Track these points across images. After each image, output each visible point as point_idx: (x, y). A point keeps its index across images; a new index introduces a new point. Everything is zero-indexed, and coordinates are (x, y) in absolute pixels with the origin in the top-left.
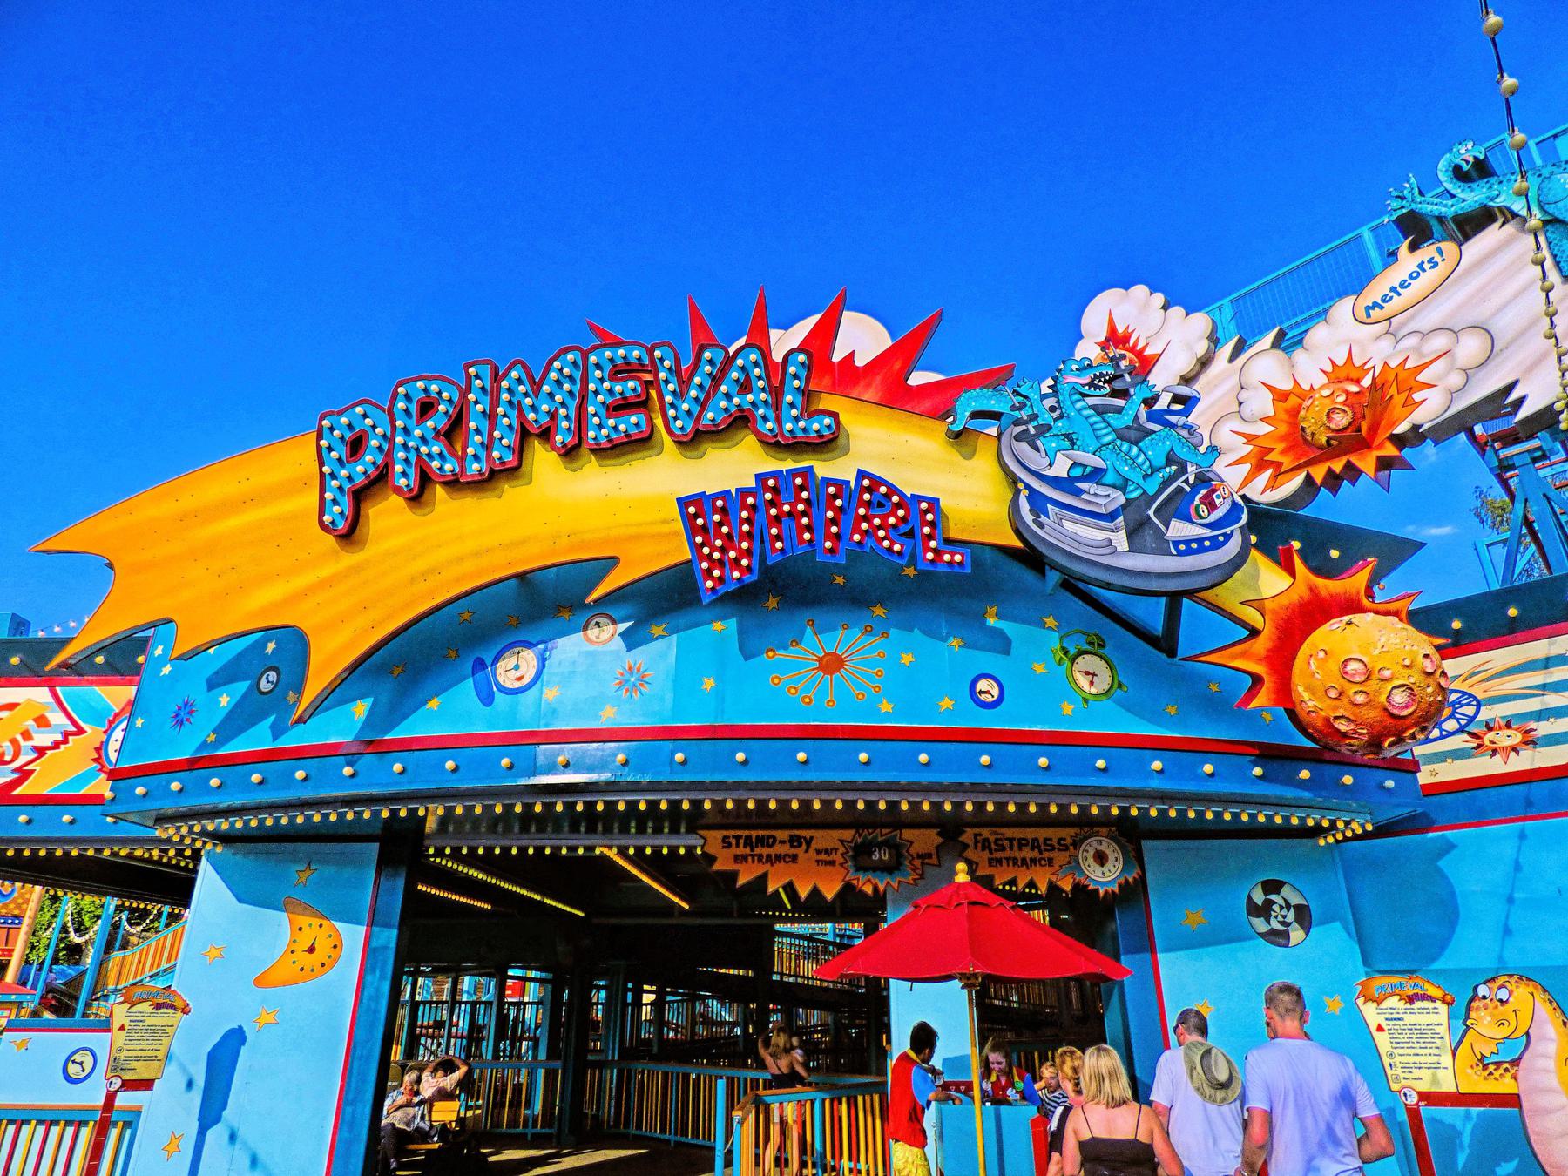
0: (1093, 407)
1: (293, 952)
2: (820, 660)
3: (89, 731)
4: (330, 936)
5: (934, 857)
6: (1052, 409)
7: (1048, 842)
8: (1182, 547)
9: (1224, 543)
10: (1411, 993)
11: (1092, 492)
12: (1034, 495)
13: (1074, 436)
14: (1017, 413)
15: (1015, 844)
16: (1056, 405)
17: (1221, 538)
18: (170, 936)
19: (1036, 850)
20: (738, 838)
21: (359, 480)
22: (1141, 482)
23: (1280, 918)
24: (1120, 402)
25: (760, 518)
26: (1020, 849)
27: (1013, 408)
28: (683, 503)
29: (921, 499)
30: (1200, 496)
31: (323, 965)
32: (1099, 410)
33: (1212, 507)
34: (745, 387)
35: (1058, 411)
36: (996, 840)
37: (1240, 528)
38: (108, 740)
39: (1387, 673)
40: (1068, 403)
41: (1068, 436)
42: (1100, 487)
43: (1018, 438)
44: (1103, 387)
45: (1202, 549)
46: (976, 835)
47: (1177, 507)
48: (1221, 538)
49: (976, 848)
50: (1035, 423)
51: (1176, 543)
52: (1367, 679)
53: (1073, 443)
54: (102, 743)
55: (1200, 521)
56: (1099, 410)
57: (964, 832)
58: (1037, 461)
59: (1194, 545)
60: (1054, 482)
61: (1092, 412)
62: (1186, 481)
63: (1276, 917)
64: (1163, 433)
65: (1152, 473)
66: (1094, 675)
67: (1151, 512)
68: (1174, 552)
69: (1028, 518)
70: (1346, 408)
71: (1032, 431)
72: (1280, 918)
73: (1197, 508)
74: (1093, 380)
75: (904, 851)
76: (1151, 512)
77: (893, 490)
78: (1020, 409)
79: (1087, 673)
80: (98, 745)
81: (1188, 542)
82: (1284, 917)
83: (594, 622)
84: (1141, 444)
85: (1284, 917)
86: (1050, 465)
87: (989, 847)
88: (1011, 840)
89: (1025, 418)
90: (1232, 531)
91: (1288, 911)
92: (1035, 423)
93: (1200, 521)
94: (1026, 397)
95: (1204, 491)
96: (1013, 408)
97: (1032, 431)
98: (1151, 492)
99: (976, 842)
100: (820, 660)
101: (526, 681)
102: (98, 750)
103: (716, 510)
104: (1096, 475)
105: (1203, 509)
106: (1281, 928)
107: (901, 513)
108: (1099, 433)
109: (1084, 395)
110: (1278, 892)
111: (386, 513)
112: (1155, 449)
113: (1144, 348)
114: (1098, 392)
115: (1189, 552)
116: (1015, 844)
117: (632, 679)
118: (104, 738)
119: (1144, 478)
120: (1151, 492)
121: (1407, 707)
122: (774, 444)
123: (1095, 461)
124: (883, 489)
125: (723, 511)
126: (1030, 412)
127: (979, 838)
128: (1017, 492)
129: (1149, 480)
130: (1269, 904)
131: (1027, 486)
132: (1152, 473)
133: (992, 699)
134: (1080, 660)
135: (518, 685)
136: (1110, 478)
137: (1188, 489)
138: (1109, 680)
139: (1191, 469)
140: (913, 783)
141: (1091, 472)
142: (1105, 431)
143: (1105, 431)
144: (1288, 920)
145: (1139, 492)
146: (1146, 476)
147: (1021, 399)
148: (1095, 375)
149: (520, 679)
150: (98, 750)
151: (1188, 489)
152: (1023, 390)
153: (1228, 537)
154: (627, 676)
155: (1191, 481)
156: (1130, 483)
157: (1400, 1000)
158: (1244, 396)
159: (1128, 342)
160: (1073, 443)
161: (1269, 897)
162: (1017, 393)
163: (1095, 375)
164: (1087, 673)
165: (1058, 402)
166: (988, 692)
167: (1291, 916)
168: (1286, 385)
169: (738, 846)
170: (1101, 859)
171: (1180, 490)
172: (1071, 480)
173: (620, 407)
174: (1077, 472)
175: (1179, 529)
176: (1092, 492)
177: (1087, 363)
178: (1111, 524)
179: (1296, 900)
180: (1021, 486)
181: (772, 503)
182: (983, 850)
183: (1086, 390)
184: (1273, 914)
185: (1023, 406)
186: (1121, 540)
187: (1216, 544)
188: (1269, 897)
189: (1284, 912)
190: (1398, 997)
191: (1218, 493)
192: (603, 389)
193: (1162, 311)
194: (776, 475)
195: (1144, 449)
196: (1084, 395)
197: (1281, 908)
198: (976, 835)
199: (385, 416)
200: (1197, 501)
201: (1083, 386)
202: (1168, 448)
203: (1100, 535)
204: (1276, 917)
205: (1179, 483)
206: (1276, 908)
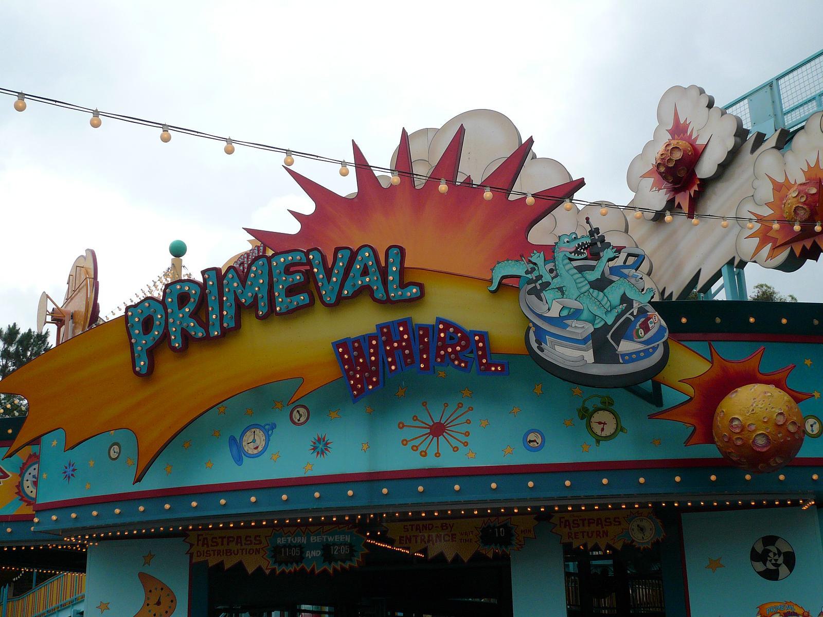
0: (576, 268)
1: (148, 605)
2: (431, 427)
3: (11, 475)
4: (168, 595)
5: (532, 532)
6: (551, 271)
7: (617, 520)
8: (627, 357)
9: (653, 353)
10: (786, 611)
11: (573, 326)
12: (538, 328)
13: (564, 289)
14: (529, 276)
15: (586, 522)
16: (554, 268)
17: (651, 350)
18: (77, 595)
19: (600, 525)
20: (412, 526)
21: (150, 344)
22: (604, 317)
23: (773, 562)
24: (593, 263)
25: (381, 352)
26: (589, 526)
27: (527, 273)
28: (337, 345)
29: (476, 333)
30: (640, 323)
31: (167, 612)
32: (580, 269)
33: (647, 329)
34: (365, 272)
35: (555, 272)
36: (574, 521)
37: (663, 342)
38: (23, 480)
39: (753, 427)
40: (561, 266)
41: (561, 289)
42: (578, 322)
43: (530, 292)
44: (583, 253)
45: (639, 358)
46: (560, 518)
47: (623, 332)
48: (651, 350)
49: (560, 527)
50: (540, 282)
51: (623, 355)
52: (742, 431)
53: (563, 293)
54: (19, 482)
55: (639, 340)
56: (580, 269)
57: (553, 516)
58: (541, 308)
59: (634, 356)
60: (550, 320)
61: (576, 271)
62: (632, 314)
63: (770, 561)
64: (619, 282)
65: (611, 310)
66: (605, 424)
67: (609, 337)
68: (621, 361)
69: (534, 345)
70: (805, 207)
71: (539, 287)
72: (773, 562)
73: (637, 331)
74: (577, 248)
75: (513, 532)
76: (609, 337)
77: (458, 329)
78: (531, 273)
79: (600, 423)
80: (17, 484)
81: (630, 354)
82: (776, 560)
83: (296, 411)
84: (605, 291)
85: (776, 560)
86: (549, 310)
87: (569, 525)
88: (583, 520)
89: (534, 278)
90: (658, 345)
91: (779, 557)
92: (540, 282)
93: (639, 340)
94: (535, 264)
95: (642, 320)
96: (527, 273)
97: (539, 287)
98: (610, 323)
99: (561, 522)
100: (431, 427)
101: (260, 449)
102: (18, 487)
103: (355, 349)
104: (575, 314)
105: (641, 331)
106: (773, 568)
107: (463, 343)
108: (580, 285)
109: (571, 260)
110: (773, 544)
111: (167, 365)
112: (614, 294)
113: (696, 138)
114: (580, 257)
115: (633, 361)
116: (586, 522)
117: (321, 446)
118: (20, 479)
119: (606, 313)
120: (610, 323)
121: (764, 447)
122: (387, 303)
123: (576, 305)
124: (451, 330)
125: (359, 349)
126: (538, 274)
127: (562, 520)
128: (529, 328)
129: (609, 315)
130: (767, 552)
131: (534, 325)
132: (611, 310)
133: (537, 445)
134: (595, 415)
135: (256, 452)
136: (585, 315)
137: (633, 319)
138: (615, 426)
139: (635, 305)
140: (614, 438)
141: (574, 313)
142: (584, 284)
143: (584, 284)
144: (778, 562)
145: (603, 323)
146: (607, 312)
147: (532, 265)
148: (578, 244)
149: (257, 448)
150: (18, 487)
151: (633, 319)
152: (533, 260)
153: (655, 349)
154: (318, 444)
155: (635, 314)
156: (597, 317)
157: (780, 615)
158: (756, 183)
159: (687, 132)
160: (563, 293)
161: (767, 547)
162: (530, 262)
163: (578, 244)
164: (600, 423)
165: (555, 266)
166: (535, 441)
167: (781, 560)
168: (780, 179)
169: (412, 530)
170: (642, 529)
171: (628, 319)
172: (561, 318)
173: (291, 291)
174: (565, 313)
175: (625, 346)
176: (573, 326)
177: (574, 236)
178: (584, 346)
179: (785, 549)
180: (531, 325)
181: (386, 343)
182: (565, 527)
183: (572, 256)
184: (769, 558)
185: (533, 270)
186: (589, 356)
187: (647, 354)
188: (767, 547)
189: (777, 557)
190: (779, 614)
191: (651, 320)
192: (282, 283)
193: (707, 109)
194: (387, 326)
195: (607, 294)
196: (571, 260)
197: (775, 554)
198: (560, 518)
199: (160, 307)
200: (638, 327)
201: (571, 253)
202: (621, 292)
203: (577, 353)
204: (770, 561)
205: (627, 315)
206: (771, 555)
